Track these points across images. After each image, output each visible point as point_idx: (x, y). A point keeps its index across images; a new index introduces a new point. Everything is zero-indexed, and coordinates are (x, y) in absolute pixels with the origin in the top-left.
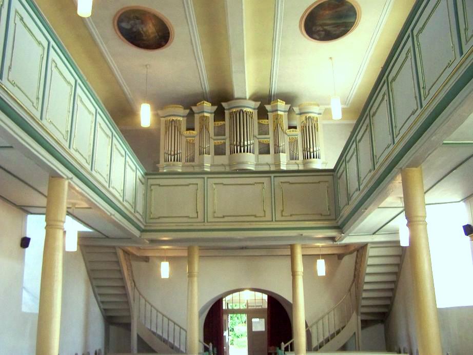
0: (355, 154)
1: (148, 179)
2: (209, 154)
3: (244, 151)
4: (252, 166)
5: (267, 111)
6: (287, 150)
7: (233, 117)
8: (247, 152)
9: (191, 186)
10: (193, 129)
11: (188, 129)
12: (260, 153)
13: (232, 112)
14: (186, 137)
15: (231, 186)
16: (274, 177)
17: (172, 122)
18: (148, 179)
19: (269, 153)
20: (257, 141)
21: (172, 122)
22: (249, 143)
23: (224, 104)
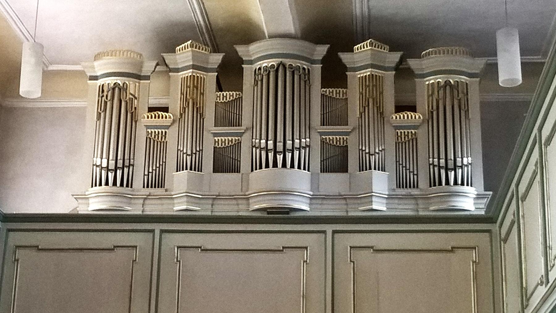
0: (538, 177)
1: (9, 230)
2: (383, 170)
3: (284, 165)
4: (304, 200)
5: (346, 67)
6: (390, 163)
7: (262, 80)
8: (292, 166)
9: (119, 251)
10: (413, 109)
11: (399, 109)
12: (325, 169)
13: (260, 69)
14: (396, 128)
15: (264, 255)
16: (334, 232)
17: (114, 89)
18: (9, 230)
19: (347, 171)
20: (317, 140)
21: (114, 89)
22: (297, 145)
23: (241, 50)
